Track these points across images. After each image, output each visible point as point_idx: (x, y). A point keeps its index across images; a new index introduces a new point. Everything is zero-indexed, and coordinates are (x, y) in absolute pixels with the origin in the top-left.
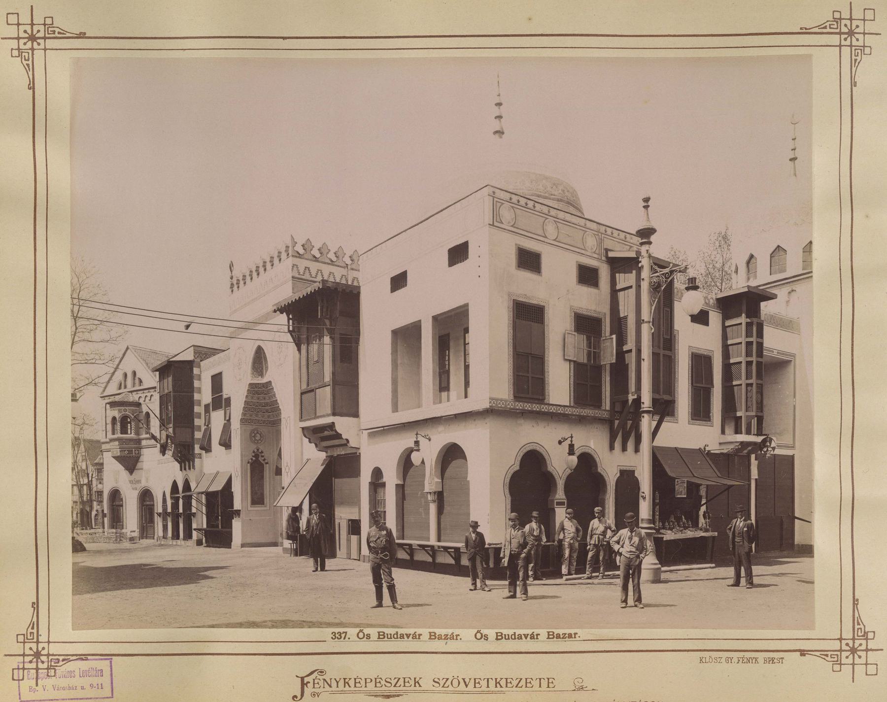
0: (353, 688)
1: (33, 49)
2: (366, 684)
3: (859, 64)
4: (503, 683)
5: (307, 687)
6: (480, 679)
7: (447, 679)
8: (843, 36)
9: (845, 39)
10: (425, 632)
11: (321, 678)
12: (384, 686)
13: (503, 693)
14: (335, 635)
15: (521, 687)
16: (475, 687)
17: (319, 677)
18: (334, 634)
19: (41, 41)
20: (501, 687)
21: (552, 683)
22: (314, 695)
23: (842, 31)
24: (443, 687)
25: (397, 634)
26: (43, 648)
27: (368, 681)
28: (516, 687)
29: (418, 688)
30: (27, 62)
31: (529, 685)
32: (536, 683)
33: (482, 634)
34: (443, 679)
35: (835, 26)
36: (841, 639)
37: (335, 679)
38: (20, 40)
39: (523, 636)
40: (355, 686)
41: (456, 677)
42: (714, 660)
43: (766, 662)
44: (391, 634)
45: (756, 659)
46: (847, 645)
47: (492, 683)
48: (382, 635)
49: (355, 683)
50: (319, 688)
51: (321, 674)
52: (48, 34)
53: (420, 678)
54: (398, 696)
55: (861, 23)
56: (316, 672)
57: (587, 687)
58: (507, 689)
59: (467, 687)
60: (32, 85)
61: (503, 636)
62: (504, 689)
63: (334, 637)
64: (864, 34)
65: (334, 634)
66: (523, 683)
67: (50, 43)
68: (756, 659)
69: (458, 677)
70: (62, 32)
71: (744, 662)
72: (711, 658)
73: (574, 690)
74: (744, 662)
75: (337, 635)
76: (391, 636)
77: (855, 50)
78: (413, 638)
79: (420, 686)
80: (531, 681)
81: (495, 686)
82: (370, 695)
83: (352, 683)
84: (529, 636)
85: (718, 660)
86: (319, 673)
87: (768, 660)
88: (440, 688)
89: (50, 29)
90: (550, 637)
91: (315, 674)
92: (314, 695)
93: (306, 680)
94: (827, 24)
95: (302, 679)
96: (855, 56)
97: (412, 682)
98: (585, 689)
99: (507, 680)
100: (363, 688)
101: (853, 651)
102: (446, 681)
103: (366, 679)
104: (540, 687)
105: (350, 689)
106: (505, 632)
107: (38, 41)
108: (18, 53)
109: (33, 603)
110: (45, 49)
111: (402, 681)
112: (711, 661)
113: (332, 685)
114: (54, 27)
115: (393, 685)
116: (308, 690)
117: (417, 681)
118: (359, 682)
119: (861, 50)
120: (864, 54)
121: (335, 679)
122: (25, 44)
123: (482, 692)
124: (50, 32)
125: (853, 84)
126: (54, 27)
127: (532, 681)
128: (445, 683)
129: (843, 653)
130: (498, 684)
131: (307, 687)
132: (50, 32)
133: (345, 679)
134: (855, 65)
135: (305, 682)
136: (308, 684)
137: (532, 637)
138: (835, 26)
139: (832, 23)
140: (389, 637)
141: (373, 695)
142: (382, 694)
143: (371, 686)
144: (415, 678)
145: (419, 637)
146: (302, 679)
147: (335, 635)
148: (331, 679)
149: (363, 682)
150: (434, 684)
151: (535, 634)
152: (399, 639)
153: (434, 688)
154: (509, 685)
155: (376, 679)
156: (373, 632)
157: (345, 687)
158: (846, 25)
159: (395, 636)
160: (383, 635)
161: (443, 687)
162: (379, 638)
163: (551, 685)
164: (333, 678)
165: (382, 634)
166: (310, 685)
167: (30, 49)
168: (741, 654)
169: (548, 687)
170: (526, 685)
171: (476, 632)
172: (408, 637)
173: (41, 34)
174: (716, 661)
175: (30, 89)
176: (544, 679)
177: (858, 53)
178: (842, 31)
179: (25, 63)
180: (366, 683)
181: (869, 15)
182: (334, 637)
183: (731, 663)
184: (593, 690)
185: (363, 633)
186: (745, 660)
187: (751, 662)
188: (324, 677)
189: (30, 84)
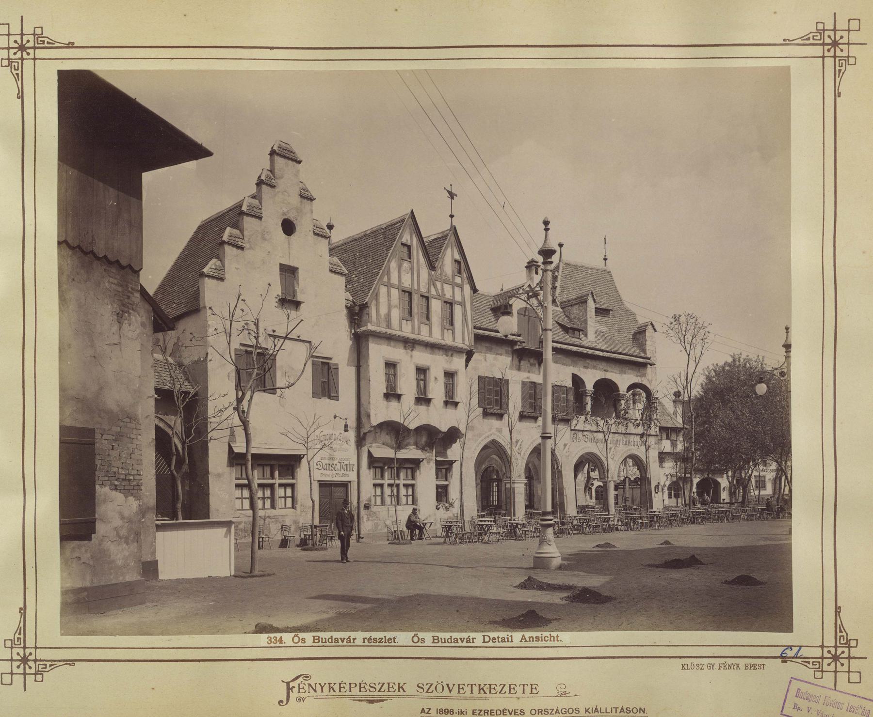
0: (338, 693)
5: (292, 692)
7: (432, 685)
8: (826, 47)
9: (829, 50)
11: (306, 682)
12: (368, 691)
14: (270, 640)
15: (384, 691)
16: (459, 692)
17: (304, 682)
19: (31, 51)
20: (485, 693)
22: (299, 700)
23: (825, 42)
24: (427, 692)
25: (451, 639)
27: (353, 685)
28: (500, 693)
29: (402, 693)
30: (17, 72)
31: (512, 691)
32: (519, 689)
33: (419, 638)
36: (822, 647)
37: (320, 684)
40: (340, 691)
44: (325, 639)
45: (738, 665)
46: (829, 652)
47: (476, 689)
49: (340, 688)
53: (404, 684)
54: (382, 701)
55: (845, 34)
58: (491, 695)
62: (488, 695)
63: (269, 642)
64: (848, 44)
66: (506, 689)
67: (40, 53)
68: (738, 665)
70: (51, 42)
73: (557, 696)
75: (273, 640)
78: (467, 642)
79: (404, 691)
83: (336, 688)
84: (465, 640)
87: (749, 667)
88: (425, 694)
89: (40, 39)
91: (301, 679)
92: (299, 699)
93: (291, 685)
94: (811, 36)
95: (288, 683)
97: (396, 687)
98: (567, 695)
100: (348, 693)
103: (350, 684)
104: (472, 693)
105: (335, 694)
110: (35, 59)
111: (386, 686)
112: (693, 668)
115: (377, 690)
116: (294, 695)
117: (481, 687)
118: (344, 687)
119: (845, 60)
121: (320, 684)
122: (15, 54)
123: (466, 698)
124: (39, 42)
128: (429, 689)
130: (401, 689)
131: (292, 692)
132: (39, 42)
133: (330, 684)
138: (819, 38)
139: (816, 34)
140: (324, 641)
143: (355, 691)
144: (399, 684)
145: (354, 641)
146: (288, 683)
148: (316, 684)
149: (347, 687)
150: (418, 689)
152: (334, 644)
154: (493, 691)
155: (360, 684)
156: (428, 636)
157: (330, 692)
158: (829, 37)
159: (449, 641)
161: (427, 692)
162: (433, 642)
164: (318, 682)
166: (296, 690)
167: (19, 59)
168: (722, 661)
169: (532, 693)
173: (31, 44)
175: (19, 98)
177: (842, 63)
178: (825, 42)
179: (14, 72)
181: (854, 25)
182: (269, 642)
186: (727, 666)
188: (309, 682)
189: (18, 94)
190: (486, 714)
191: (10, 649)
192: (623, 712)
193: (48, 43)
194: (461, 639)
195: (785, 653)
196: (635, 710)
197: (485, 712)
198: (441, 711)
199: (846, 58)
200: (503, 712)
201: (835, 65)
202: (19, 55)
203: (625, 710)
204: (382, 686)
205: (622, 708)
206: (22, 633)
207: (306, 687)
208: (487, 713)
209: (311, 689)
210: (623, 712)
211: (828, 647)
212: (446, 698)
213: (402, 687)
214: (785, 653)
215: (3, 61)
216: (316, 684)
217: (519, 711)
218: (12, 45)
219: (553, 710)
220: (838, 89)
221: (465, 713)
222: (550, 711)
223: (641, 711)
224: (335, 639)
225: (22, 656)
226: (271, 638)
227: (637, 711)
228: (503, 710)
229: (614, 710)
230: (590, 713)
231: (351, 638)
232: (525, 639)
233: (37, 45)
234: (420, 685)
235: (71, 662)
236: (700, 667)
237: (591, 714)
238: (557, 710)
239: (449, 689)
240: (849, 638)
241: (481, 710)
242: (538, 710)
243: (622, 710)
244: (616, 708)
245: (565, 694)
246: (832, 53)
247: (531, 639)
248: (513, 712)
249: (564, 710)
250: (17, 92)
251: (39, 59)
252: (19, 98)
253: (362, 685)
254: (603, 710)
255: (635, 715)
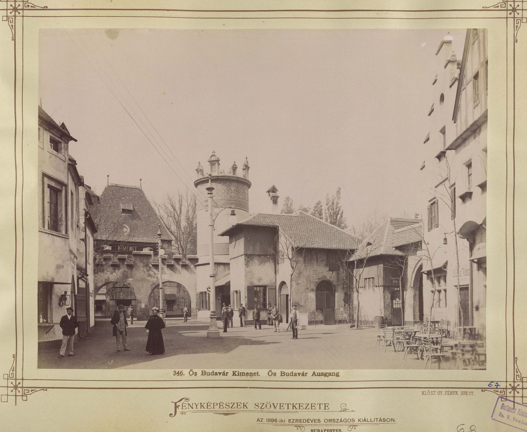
1: (15, 16)
2: (214, 407)
3: (519, 29)
4: (297, 406)
5: (178, 408)
6: (283, 404)
7: (264, 404)
8: (509, 12)
9: (510, 14)
10: (310, 372)
12: (225, 407)
13: (297, 412)
15: (234, 408)
16: (280, 409)
17: (185, 402)
18: (175, 372)
19: (21, 11)
20: (296, 409)
21: (327, 406)
22: (182, 413)
23: (508, 9)
25: (292, 373)
26: (510, 385)
27: (215, 404)
28: (305, 409)
31: (313, 408)
32: (317, 407)
34: (232, 403)
35: (504, 6)
36: (23, 379)
37: (195, 404)
38: (8, 11)
39: (297, 374)
40: (207, 408)
41: (268, 402)
42: (430, 393)
43: (462, 394)
45: (456, 392)
46: (19, 383)
47: (291, 407)
48: (204, 373)
49: (207, 406)
50: (315, 409)
51: (187, 400)
52: (25, 7)
53: (247, 403)
54: (233, 414)
56: (184, 399)
57: (348, 409)
58: (237, 409)
59: (275, 409)
60: (14, 38)
61: (206, 373)
62: (298, 410)
63: (175, 374)
64: (523, 10)
65: (175, 372)
66: (310, 406)
67: (26, 13)
68: (456, 392)
69: (270, 402)
70: (34, 6)
71: (449, 394)
72: (429, 392)
73: (341, 411)
74: (449, 394)
76: (209, 374)
77: (517, 20)
79: (247, 408)
80: (315, 405)
81: (279, 408)
82: (217, 413)
83: (205, 406)
84: (301, 374)
85: (433, 393)
86: (186, 400)
87: (463, 393)
90: (204, 374)
93: (178, 404)
95: (176, 403)
96: (517, 24)
97: (242, 405)
98: (347, 410)
99: (325, 405)
100: (212, 409)
101: (514, 388)
102: (263, 405)
103: (214, 403)
104: (288, 409)
105: (204, 409)
106: (208, 371)
107: (19, 11)
108: (6, 19)
109: (482, 391)
110: (23, 16)
113: (193, 407)
114: (29, 3)
115: (231, 407)
118: (210, 406)
119: (520, 20)
120: (522, 23)
121: (195, 404)
122: (11, 13)
123: (285, 412)
124: (26, 6)
125: (515, 41)
126: (29, 3)
127: (315, 406)
128: (262, 407)
129: (15, 380)
130: (245, 406)
131: (178, 408)
132: (26, 6)
133: (201, 403)
134: (516, 29)
135: (177, 406)
136: (179, 407)
137: (303, 375)
138: (504, 6)
141: (218, 413)
142: (223, 413)
143: (217, 408)
144: (244, 403)
145: (227, 374)
146: (176, 403)
147: (175, 373)
148: (193, 404)
149: (212, 406)
151: (304, 373)
153: (256, 409)
154: (301, 408)
155: (220, 403)
157: (201, 408)
160: (205, 373)
163: (327, 408)
164: (194, 403)
165: (204, 372)
166: (180, 407)
168: (447, 390)
169: (325, 409)
170: (312, 407)
171: (269, 371)
172: (299, 375)
173: (21, 7)
174: (432, 394)
175: (13, 40)
176: (322, 404)
177: (518, 22)
178: (508, 9)
179: (10, 24)
180: (214, 406)
182: (175, 374)
183: (454, 394)
184: (352, 411)
185: (192, 371)
186: (450, 393)
187: (453, 394)
189: (13, 37)
190: (297, 422)
191: (24, 381)
192: (381, 421)
193: (32, 7)
194: (298, 373)
195: (491, 385)
196: (388, 420)
197: (296, 421)
198: (269, 420)
199: (521, 19)
200: (308, 421)
201: (514, 23)
202: (13, 13)
203: (382, 420)
204: (306, 407)
205: (380, 419)
206: (15, 370)
207: (187, 406)
208: (297, 421)
209: (191, 405)
210: (381, 421)
211: (13, 379)
212: (273, 412)
213: (295, 406)
214: (491, 385)
215: (4, 17)
216: (193, 404)
217: (317, 420)
218: (9, 7)
219: (338, 419)
220: (516, 38)
221: (284, 421)
222: (336, 421)
223: (392, 421)
224: (215, 373)
225: (512, 390)
226: (176, 372)
227: (390, 420)
228: (308, 419)
229: (376, 420)
230: (361, 422)
231: (225, 372)
232: (315, 374)
233: (24, 8)
234: (256, 404)
235: (45, 389)
236: (433, 393)
237: (362, 423)
238: (341, 420)
239: (274, 406)
240: (522, 376)
241: (294, 420)
242: (329, 420)
243: (380, 420)
244: (377, 419)
245: (345, 410)
246: (512, 15)
247: (251, 374)
248: (314, 420)
249: (345, 420)
250: (12, 36)
251: (26, 16)
252: (13, 40)
253: (221, 404)
254: (369, 420)
255: (388, 423)
